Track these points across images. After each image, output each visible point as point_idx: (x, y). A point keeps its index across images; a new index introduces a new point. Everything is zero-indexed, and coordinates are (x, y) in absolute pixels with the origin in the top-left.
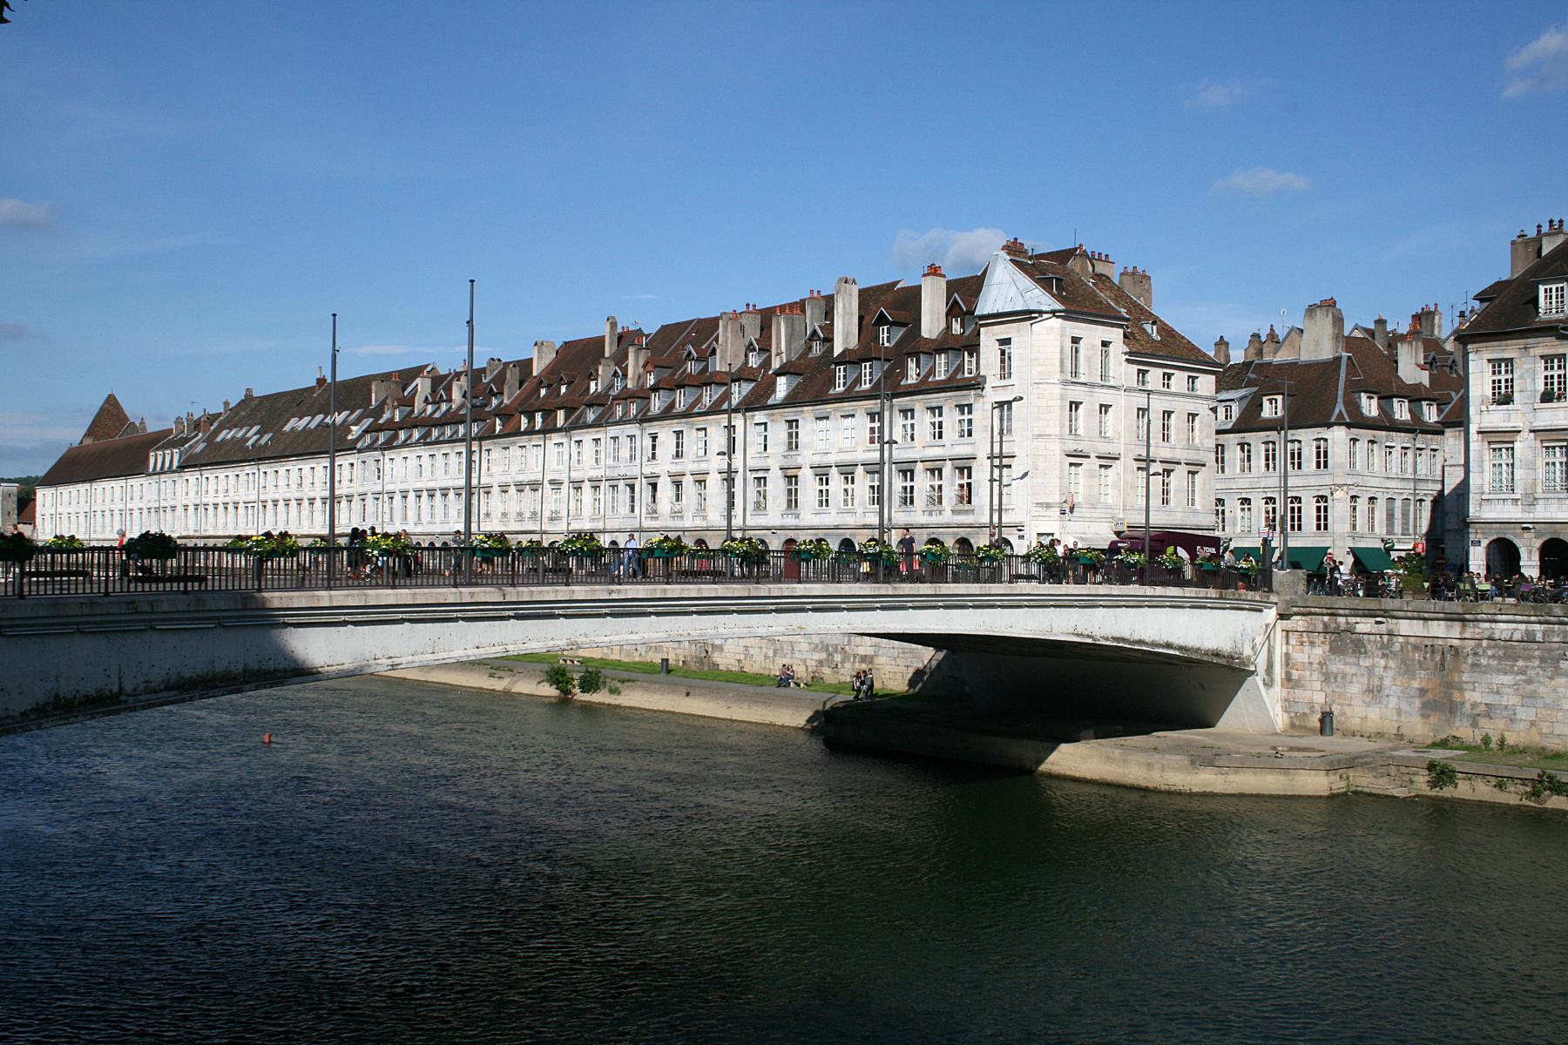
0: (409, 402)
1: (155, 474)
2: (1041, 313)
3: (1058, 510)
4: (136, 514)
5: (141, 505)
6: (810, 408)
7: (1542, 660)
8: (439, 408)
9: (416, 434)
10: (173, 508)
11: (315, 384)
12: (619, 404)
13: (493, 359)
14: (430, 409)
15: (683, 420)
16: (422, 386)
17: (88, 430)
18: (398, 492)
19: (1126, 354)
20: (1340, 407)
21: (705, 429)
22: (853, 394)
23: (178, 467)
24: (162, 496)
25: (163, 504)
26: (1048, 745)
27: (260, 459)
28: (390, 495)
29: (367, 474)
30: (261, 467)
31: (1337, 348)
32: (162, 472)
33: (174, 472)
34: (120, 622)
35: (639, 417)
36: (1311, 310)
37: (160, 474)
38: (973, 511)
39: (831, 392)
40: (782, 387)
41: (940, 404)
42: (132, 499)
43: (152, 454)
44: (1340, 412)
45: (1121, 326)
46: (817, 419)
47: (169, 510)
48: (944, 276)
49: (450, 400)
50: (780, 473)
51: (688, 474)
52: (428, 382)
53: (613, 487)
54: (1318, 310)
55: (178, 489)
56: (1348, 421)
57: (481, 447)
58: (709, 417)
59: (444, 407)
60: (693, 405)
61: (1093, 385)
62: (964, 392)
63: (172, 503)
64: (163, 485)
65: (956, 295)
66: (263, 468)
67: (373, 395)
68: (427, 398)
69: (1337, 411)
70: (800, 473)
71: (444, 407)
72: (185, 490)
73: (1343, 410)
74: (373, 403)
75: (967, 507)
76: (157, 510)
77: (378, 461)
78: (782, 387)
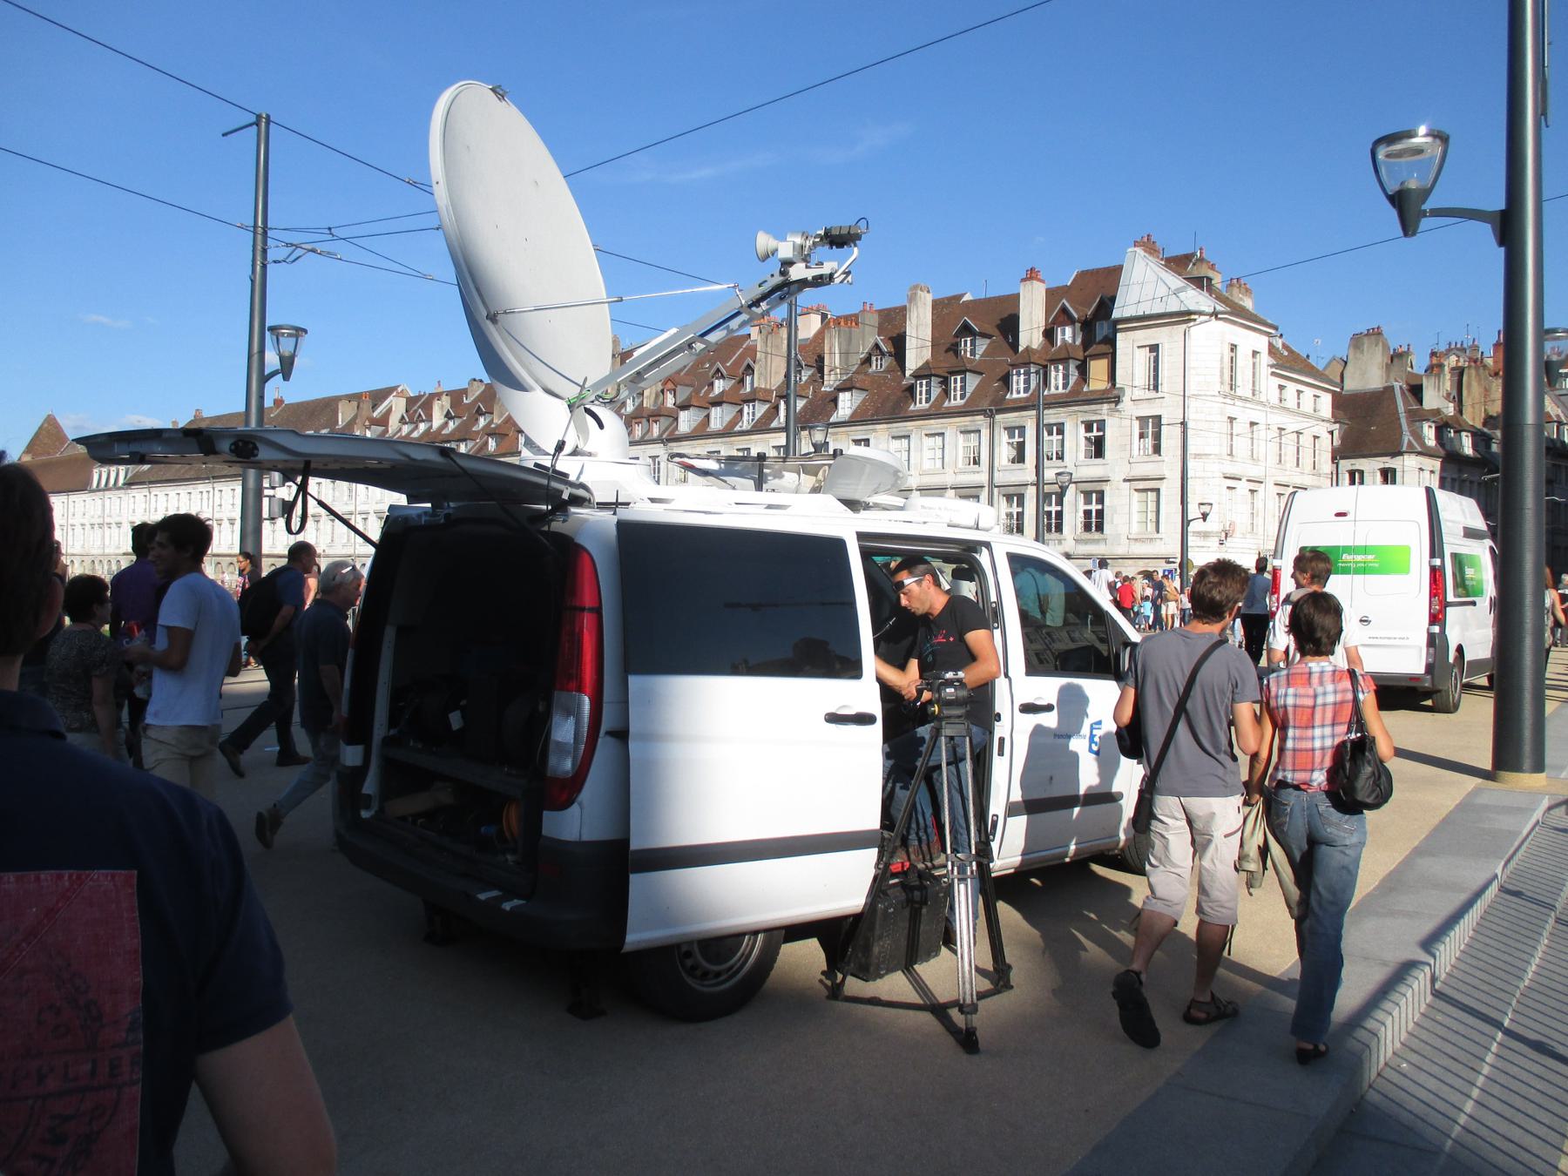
0: (383, 421)
1: (99, 491)
2: (1200, 313)
3: (1217, 539)
4: (78, 529)
5: (83, 521)
6: (885, 426)
7: (1288, 685)
8: (416, 428)
9: (656, 430)
10: (119, 524)
11: (272, 405)
12: (638, 423)
13: (475, 380)
14: (406, 429)
15: (720, 440)
16: (397, 405)
17: (27, 447)
18: (226, 519)
19: (1272, 366)
20: (1407, 437)
21: (942, 434)
22: (943, 410)
23: (124, 484)
24: (107, 512)
25: (108, 520)
26: (1088, 792)
27: (151, 482)
28: (364, 516)
29: (337, 494)
30: (215, 485)
31: (1388, 376)
32: (107, 488)
33: (120, 489)
34: (1552, 870)
35: (664, 436)
36: (1357, 341)
37: (104, 490)
38: (1105, 540)
39: (912, 407)
40: (847, 404)
41: (1022, 424)
42: (156, 511)
43: (95, 470)
44: (1409, 441)
45: (1268, 334)
46: (893, 438)
47: (114, 526)
48: (1043, 281)
49: (430, 419)
50: (228, 522)
51: (372, 512)
52: (403, 402)
53: (1252, 491)
54: (1366, 340)
55: (124, 505)
56: (1420, 450)
57: (214, 488)
58: (753, 437)
59: (422, 427)
60: (734, 422)
61: (1246, 400)
62: (1093, 407)
63: (118, 519)
64: (107, 502)
65: (1064, 301)
66: (218, 486)
67: (340, 415)
68: (403, 417)
69: (1406, 442)
70: (1107, 488)
71: (422, 427)
72: (132, 506)
73: (1411, 438)
74: (340, 423)
75: (1097, 535)
76: (101, 525)
77: (146, 496)
78: (847, 404)
